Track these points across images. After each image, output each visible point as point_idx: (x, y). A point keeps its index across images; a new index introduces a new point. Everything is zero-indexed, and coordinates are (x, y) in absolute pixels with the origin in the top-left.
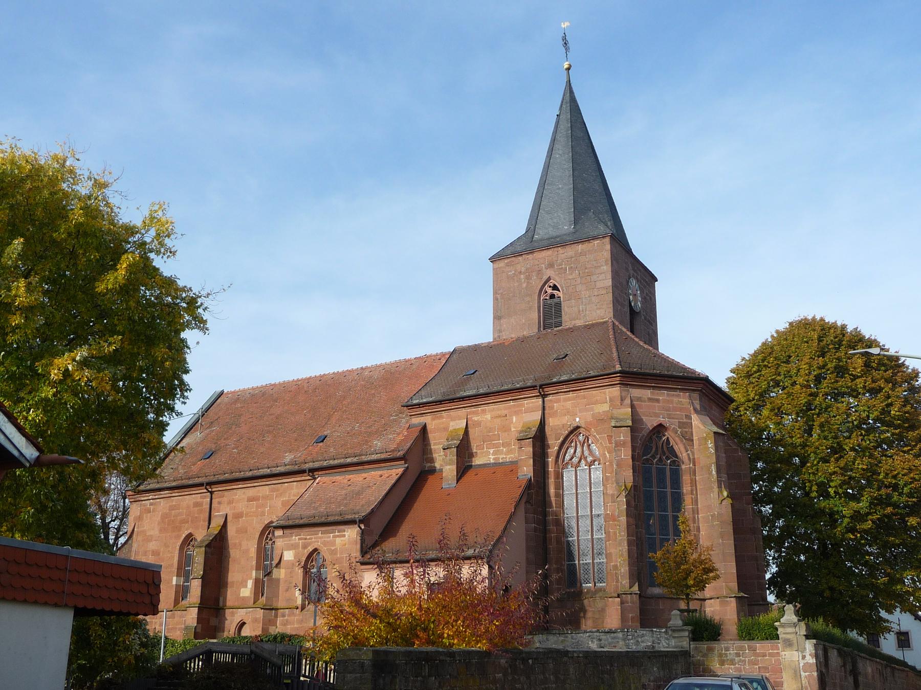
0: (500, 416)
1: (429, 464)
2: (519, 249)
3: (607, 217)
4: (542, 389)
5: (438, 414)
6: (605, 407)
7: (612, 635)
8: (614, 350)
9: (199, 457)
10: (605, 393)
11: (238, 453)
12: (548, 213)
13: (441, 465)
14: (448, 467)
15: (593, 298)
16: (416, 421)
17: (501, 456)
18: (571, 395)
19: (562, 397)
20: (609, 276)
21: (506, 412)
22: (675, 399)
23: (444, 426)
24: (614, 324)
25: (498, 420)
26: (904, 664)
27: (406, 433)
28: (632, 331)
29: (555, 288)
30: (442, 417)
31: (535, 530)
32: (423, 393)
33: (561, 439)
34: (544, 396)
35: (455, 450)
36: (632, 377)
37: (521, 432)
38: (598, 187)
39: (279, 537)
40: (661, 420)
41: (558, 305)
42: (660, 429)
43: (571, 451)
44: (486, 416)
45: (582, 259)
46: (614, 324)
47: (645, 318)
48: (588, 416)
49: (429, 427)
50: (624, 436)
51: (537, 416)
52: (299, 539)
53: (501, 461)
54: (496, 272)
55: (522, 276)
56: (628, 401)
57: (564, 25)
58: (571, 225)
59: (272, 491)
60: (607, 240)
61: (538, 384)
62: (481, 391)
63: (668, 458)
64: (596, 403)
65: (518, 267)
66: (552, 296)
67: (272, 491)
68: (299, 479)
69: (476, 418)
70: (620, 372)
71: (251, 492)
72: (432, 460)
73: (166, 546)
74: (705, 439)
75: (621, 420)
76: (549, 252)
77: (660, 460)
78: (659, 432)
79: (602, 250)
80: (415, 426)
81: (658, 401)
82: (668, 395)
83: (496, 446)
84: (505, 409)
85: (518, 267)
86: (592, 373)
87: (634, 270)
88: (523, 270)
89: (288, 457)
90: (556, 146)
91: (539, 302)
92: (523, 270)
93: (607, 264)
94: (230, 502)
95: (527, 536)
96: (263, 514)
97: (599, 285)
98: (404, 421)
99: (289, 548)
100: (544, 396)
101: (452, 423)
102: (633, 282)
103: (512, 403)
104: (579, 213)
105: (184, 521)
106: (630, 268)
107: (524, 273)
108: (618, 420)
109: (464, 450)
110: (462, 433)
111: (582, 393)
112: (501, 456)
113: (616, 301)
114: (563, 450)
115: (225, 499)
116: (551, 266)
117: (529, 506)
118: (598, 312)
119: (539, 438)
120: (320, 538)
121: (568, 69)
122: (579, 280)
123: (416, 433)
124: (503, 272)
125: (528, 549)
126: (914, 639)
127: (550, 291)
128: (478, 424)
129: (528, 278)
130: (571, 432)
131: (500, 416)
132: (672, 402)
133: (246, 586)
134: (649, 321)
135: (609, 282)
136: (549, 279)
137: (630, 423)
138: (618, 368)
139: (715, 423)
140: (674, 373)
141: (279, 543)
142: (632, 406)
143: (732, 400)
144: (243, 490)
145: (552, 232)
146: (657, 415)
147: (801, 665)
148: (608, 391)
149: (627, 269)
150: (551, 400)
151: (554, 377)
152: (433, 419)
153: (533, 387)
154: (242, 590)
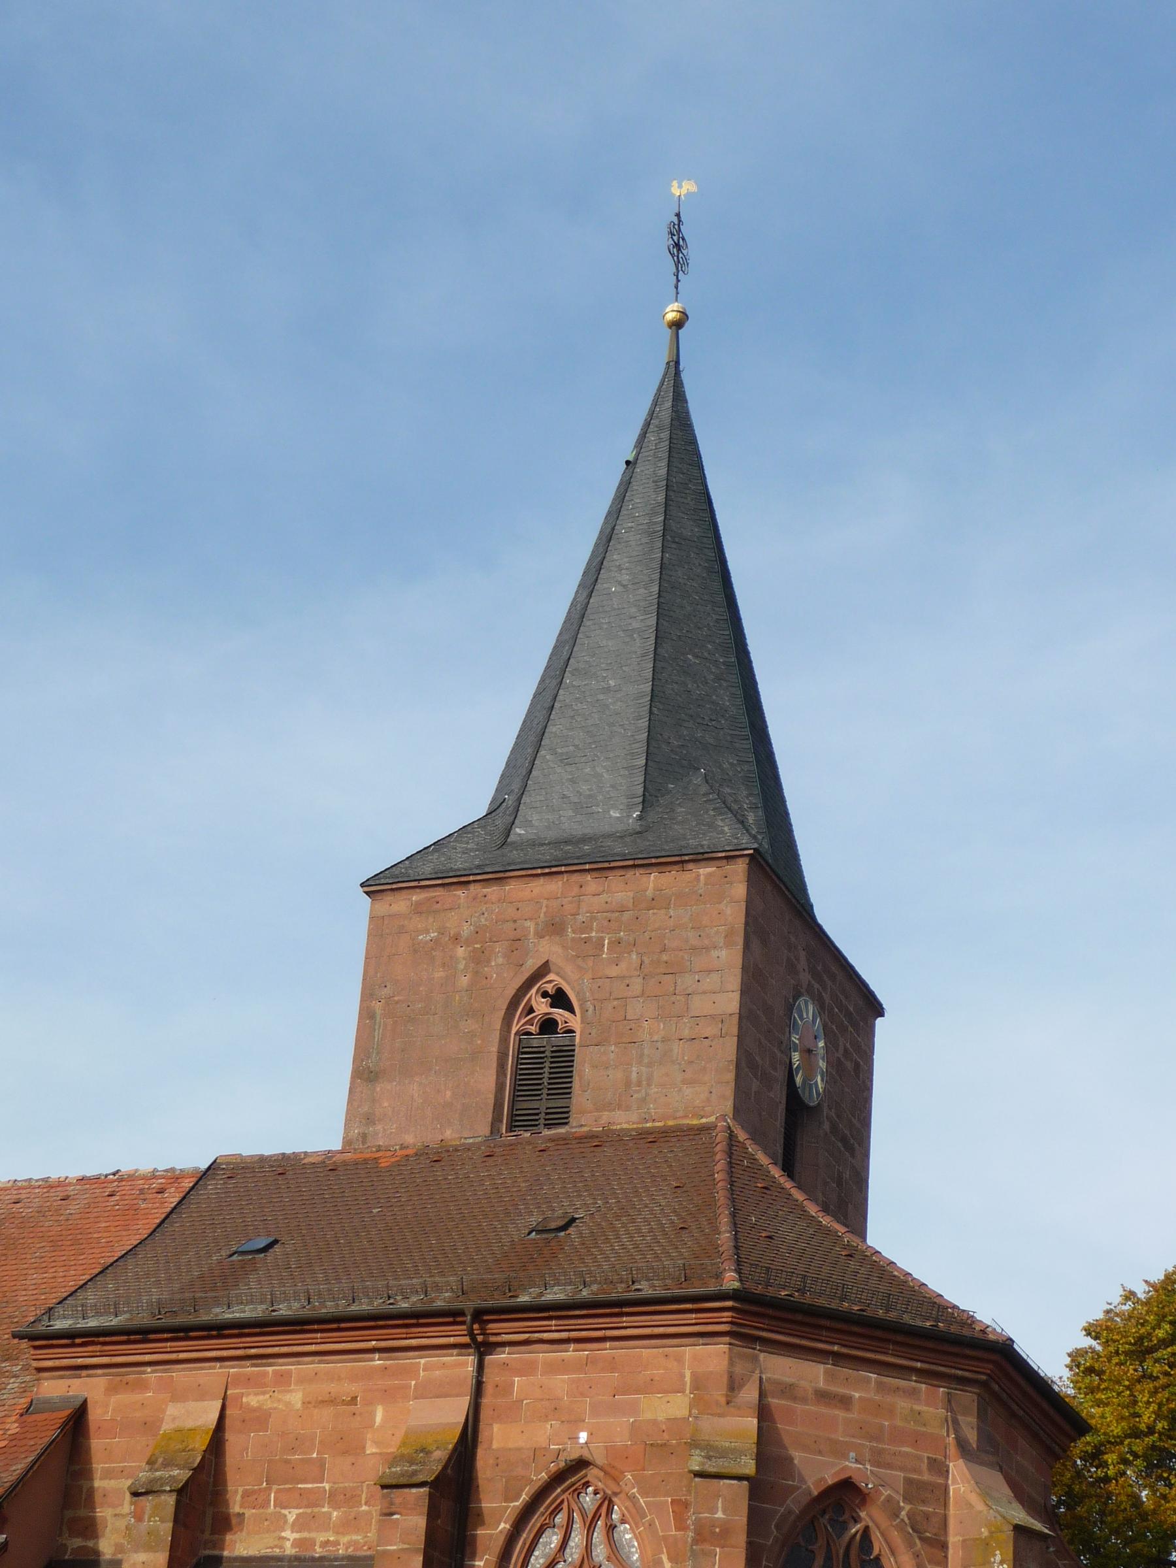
0: (332, 1401)
1: (77, 1542)
2: (460, 863)
3: (747, 799)
4: (481, 1324)
5: (132, 1375)
6: (676, 1406)
8: (724, 1221)
10: (679, 1360)
12: (566, 760)
13: (119, 1548)
14: (141, 1557)
15: (676, 1048)
16: (55, 1388)
17: (321, 1537)
18: (571, 1353)
19: (542, 1356)
20: (734, 981)
22: (903, 1404)
23: (149, 1415)
24: (732, 1136)
25: (327, 1413)
27: (14, 1428)
28: (788, 1168)
29: (560, 999)
30: (142, 1386)
32: (90, 1297)
33: (524, 1497)
34: (483, 1349)
35: (171, 1500)
36: (769, 1316)
37: (395, 1460)
38: (728, 699)
40: (851, 1466)
41: (564, 1058)
42: (844, 1495)
43: (552, 1540)
44: (288, 1395)
45: (656, 918)
46: (732, 1136)
47: (834, 1128)
48: (619, 1428)
49: (95, 1415)
50: (727, 1507)
51: (454, 1412)
53: (318, 1552)
54: (377, 925)
55: (461, 952)
56: (750, 1394)
58: (630, 807)
60: (740, 868)
61: (469, 1304)
62: (283, 1311)
64: (649, 1387)
65: (452, 921)
66: (548, 1026)
70: (734, 1295)
72: (89, 1528)
74: (986, 1546)
75: (723, 1454)
76: (554, 886)
78: (840, 1508)
79: (719, 899)
80: (49, 1406)
81: (845, 1402)
82: (880, 1387)
83: (310, 1500)
85: (452, 921)
86: (646, 1289)
88: (466, 930)
91: (504, 1040)
92: (466, 930)
93: (729, 944)
97: (699, 1005)
98: (13, 1384)
100: (483, 1349)
101: (172, 1410)
102: (808, 1011)
103: (377, 1361)
104: (661, 772)
106: (803, 964)
107: (468, 942)
108: (711, 1451)
109: (200, 1504)
110: (201, 1443)
111: (607, 1351)
112: (321, 1537)
113: (747, 1065)
114: (526, 1536)
116: (554, 928)
118: (688, 1091)
119: (452, 1488)
121: (677, 325)
122: (637, 985)
123: (48, 1430)
124: (402, 930)
127: (542, 1007)
128: (260, 1419)
129: (479, 958)
130: (558, 1478)
131: (332, 1401)
135: (730, 1002)
136: (543, 970)
137: (748, 1466)
138: (731, 1281)
139: (1020, 1496)
140: (907, 1319)
142: (764, 1413)
143: (1081, 1427)
145: (571, 824)
146: (839, 1451)
148: (691, 1352)
149: (792, 969)
151: (524, 1288)
152: (112, 1390)
153: (452, 1316)
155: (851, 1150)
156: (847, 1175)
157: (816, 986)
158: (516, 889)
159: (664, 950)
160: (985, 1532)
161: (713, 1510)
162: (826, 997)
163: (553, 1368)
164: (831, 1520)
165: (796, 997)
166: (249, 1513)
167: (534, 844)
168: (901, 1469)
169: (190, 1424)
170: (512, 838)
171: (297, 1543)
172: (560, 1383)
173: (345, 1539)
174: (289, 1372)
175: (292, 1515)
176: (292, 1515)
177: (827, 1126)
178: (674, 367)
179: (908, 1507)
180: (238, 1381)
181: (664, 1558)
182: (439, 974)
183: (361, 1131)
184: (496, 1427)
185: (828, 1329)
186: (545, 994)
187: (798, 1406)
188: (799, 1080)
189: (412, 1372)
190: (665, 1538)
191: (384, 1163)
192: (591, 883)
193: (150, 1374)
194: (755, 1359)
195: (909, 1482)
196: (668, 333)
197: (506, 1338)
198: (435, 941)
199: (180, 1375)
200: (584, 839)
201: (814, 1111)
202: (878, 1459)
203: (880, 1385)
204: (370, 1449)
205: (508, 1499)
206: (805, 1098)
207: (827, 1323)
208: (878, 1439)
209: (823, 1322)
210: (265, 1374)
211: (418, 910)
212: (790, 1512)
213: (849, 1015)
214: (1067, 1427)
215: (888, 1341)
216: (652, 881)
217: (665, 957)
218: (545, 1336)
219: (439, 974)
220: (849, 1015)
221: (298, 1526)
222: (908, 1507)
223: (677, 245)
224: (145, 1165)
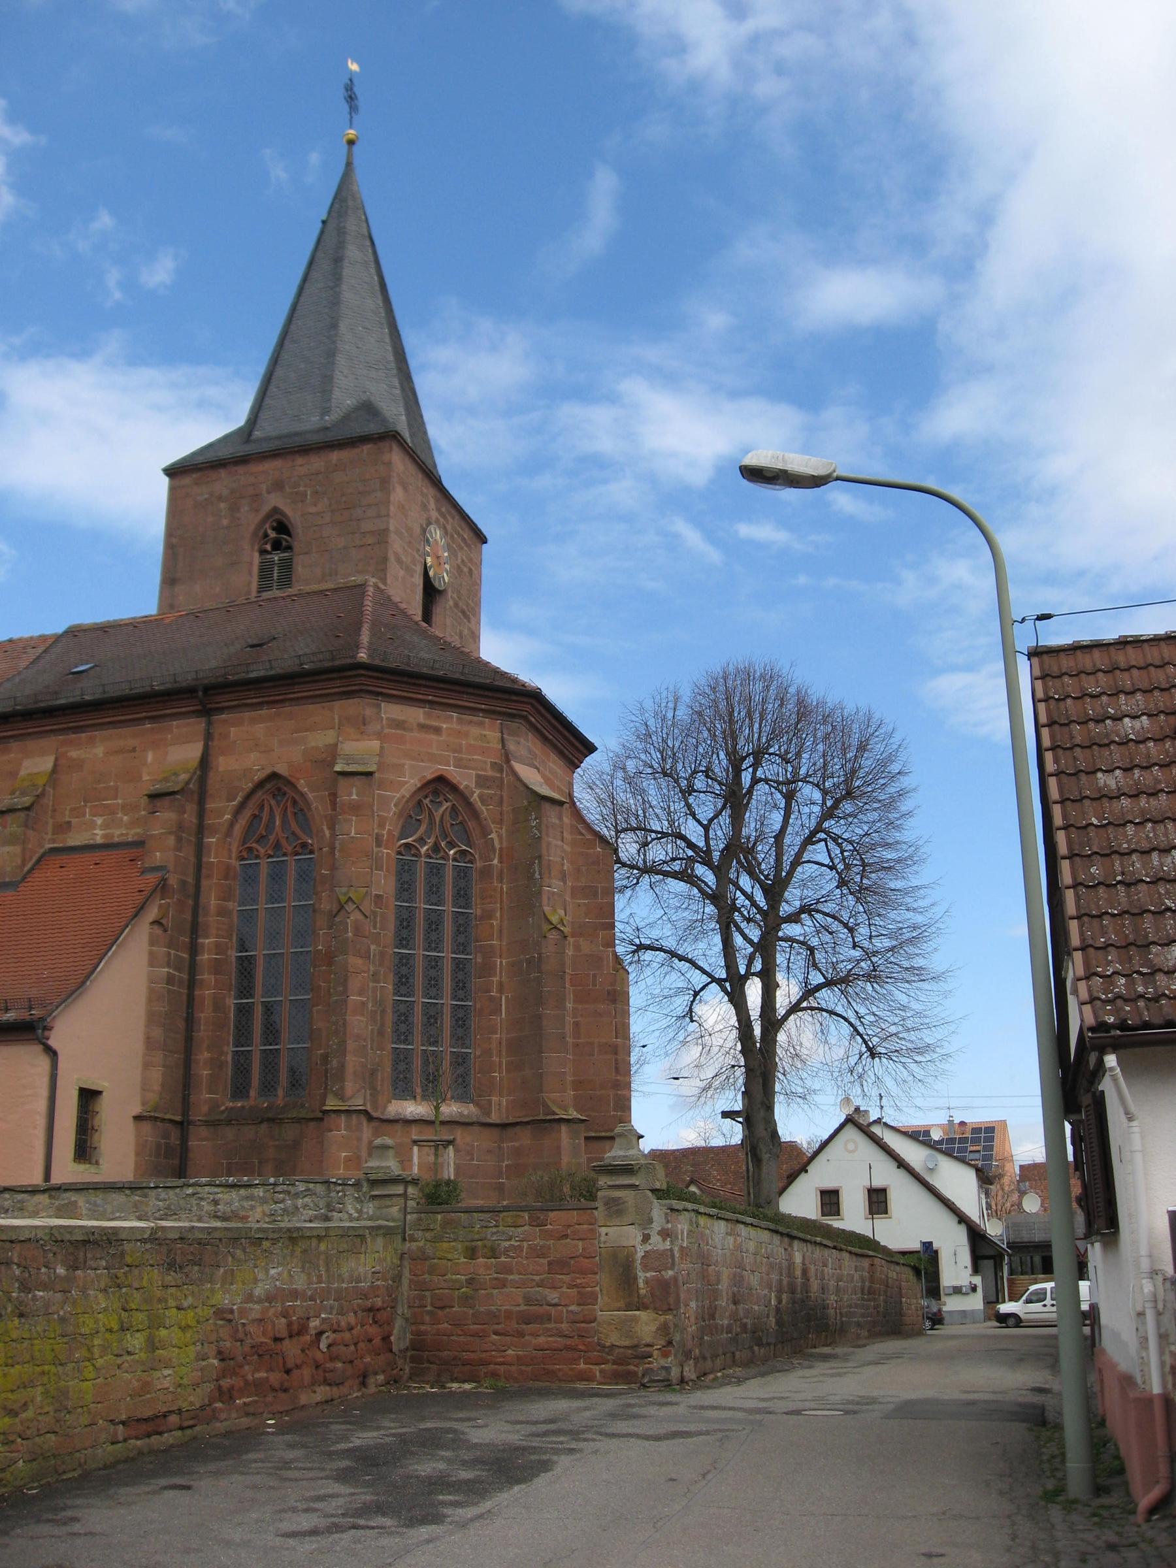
2: (224, 453)
7: (242, 1192)
17: (118, 832)
22: (475, 731)
31: (170, 980)
33: (239, 799)
34: (206, 712)
47: (456, 605)
53: (116, 840)
54: (172, 490)
55: (222, 505)
63: (451, 845)
69: (74, 754)
76: (278, 463)
77: (436, 848)
81: (437, 730)
82: (460, 721)
83: (111, 811)
87: (439, 510)
88: (225, 492)
90: (314, 275)
92: (225, 492)
95: (151, 990)
102: (436, 534)
112: (118, 832)
116: (278, 486)
117: (158, 931)
125: (152, 1019)
126: (895, 1200)
128: (78, 765)
129: (234, 508)
134: (463, 612)
147: (640, 1254)
149: (425, 507)
155: (473, 620)
156: (466, 632)
157: (442, 520)
158: (255, 468)
159: (343, 495)
161: (350, 794)
162: (449, 527)
164: (431, 801)
165: (429, 523)
166: (74, 821)
167: (268, 439)
169: (35, 771)
170: (253, 437)
171: (105, 836)
172: (259, 729)
173: (132, 832)
175: (99, 821)
176: (99, 821)
177: (451, 603)
178: (349, 164)
179: (478, 792)
181: (325, 828)
182: (210, 519)
184: (221, 759)
185: (425, 686)
187: (408, 734)
188: (431, 573)
190: (325, 816)
191: (167, 621)
192: (300, 460)
193: (14, 745)
194: (379, 706)
195: (478, 776)
196: (345, 147)
197: (227, 704)
199: (31, 744)
200: (296, 434)
201: (440, 592)
202: (459, 764)
203: (458, 719)
204: (145, 777)
205: (229, 800)
206: (436, 584)
207: (423, 682)
208: (460, 752)
209: (421, 682)
212: (403, 797)
213: (464, 539)
214: (582, 748)
215: (463, 693)
216: (335, 456)
217: (344, 499)
218: (249, 701)
219: (210, 519)
220: (464, 539)
221: (103, 827)
222: (478, 792)
223: (350, 97)
224: (26, 634)
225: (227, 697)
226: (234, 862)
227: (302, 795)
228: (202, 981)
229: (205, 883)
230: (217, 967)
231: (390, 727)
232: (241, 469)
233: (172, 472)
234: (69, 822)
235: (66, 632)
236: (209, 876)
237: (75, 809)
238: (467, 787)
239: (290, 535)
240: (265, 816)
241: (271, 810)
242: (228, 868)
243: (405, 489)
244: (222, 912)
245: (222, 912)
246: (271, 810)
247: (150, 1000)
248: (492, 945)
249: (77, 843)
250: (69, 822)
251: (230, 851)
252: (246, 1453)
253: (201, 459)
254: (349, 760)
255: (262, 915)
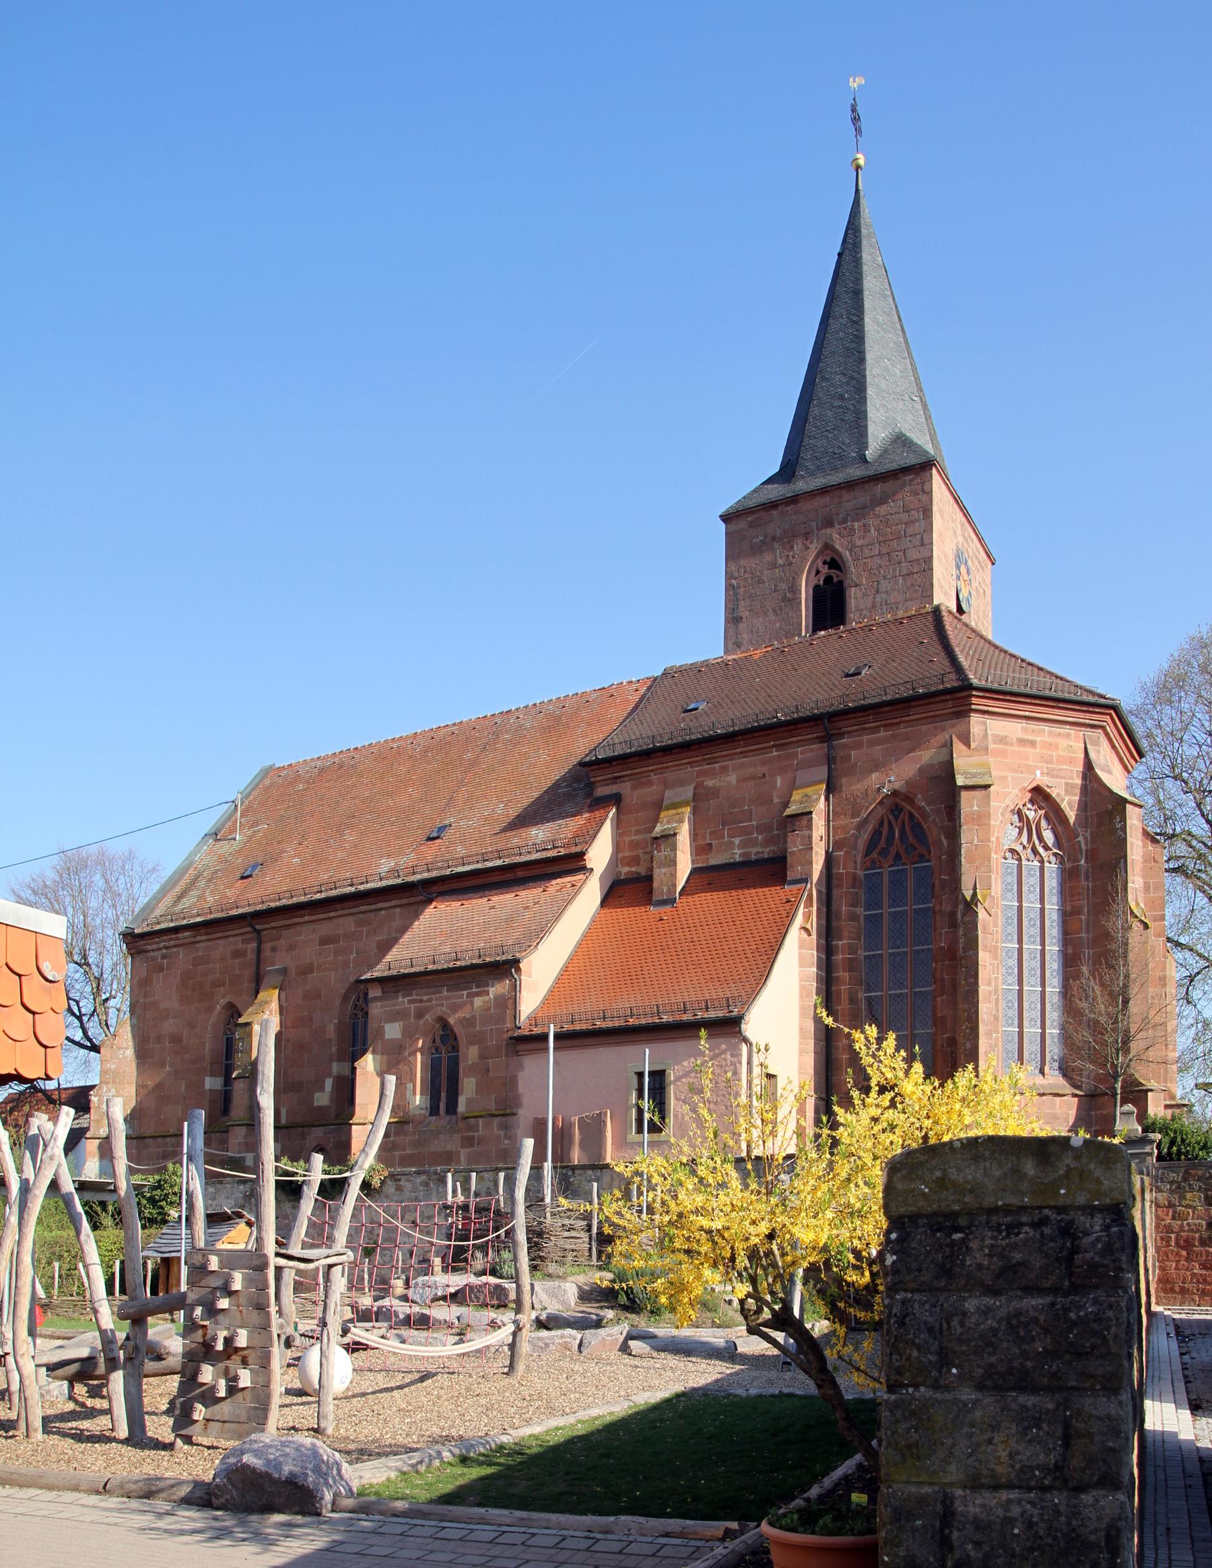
0: (753, 778)
9: (238, 875)
11: (302, 864)
17: (754, 850)
21: (764, 769)
22: (1063, 743)
26: (1130, 1173)
34: (827, 738)
39: (375, 999)
52: (410, 1002)
53: (754, 857)
57: (855, 83)
59: (360, 924)
67: (360, 924)
68: (404, 901)
69: (710, 783)
71: (325, 929)
73: (191, 1025)
75: (974, 776)
76: (826, 500)
81: (1033, 744)
83: (746, 831)
84: (763, 763)
88: (778, 533)
89: (385, 865)
90: (837, 310)
92: (778, 533)
94: (291, 948)
95: (802, 987)
96: (346, 964)
99: (393, 1017)
105: (218, 984)
106: (959, 532)
112: (754, 850)
115: (283, 942)
120: (447, 998)
128: (715, 792)
131: (753, 778)
132: (1057, 747)
133: (322, 1089)
141: (376, 1010)
144: (312, 926)
150: (845, 746)
152: (634, 788)
154: (317, 1095)
160: (1110, 806)
163: (872, 744)
168: (1064, 778)
171: (741, 855)
173: (768, 850)
174: (727, 766)
175: (737, 841)
176: (737, 841)
180: (705, 773)
183: (227, 999)
184: (844, 779)
186: (825, 563)
187: (1009, 748)
189: (796, 754)
192: (846, 496)
195: (1067, 784)
198: (763, 542)
203: (1050, 732)
208: (1051, 763)
210: (714, 768)
211: (751, 525)
225: (852, 722)
226: (861, 873)
227: (920, 809)
228: (837, 978)
229: (835, 892)
230: (851, 965)
231: (994, 742)
232: (790, 508)
233: (726, 518)
234: (710, 844)
235: (665, 674)
236: (839, 886)
237: (714, 832)
238: (1058, 795)
239: (840, 570)
240: (885, 831)
241: (890, 823)
242: (855, 877)
243: (942, 516)
244: (853, 917)
245: (853, 917)
246: (890, 823)
247: (801, 997)
248: (1081, 938)
249: (718, 862)
250: (710, 844)
251: (855, 862)
252: (493, 1474)
253: (751, 503)
254: (966, 774)
255: (886, 918)
